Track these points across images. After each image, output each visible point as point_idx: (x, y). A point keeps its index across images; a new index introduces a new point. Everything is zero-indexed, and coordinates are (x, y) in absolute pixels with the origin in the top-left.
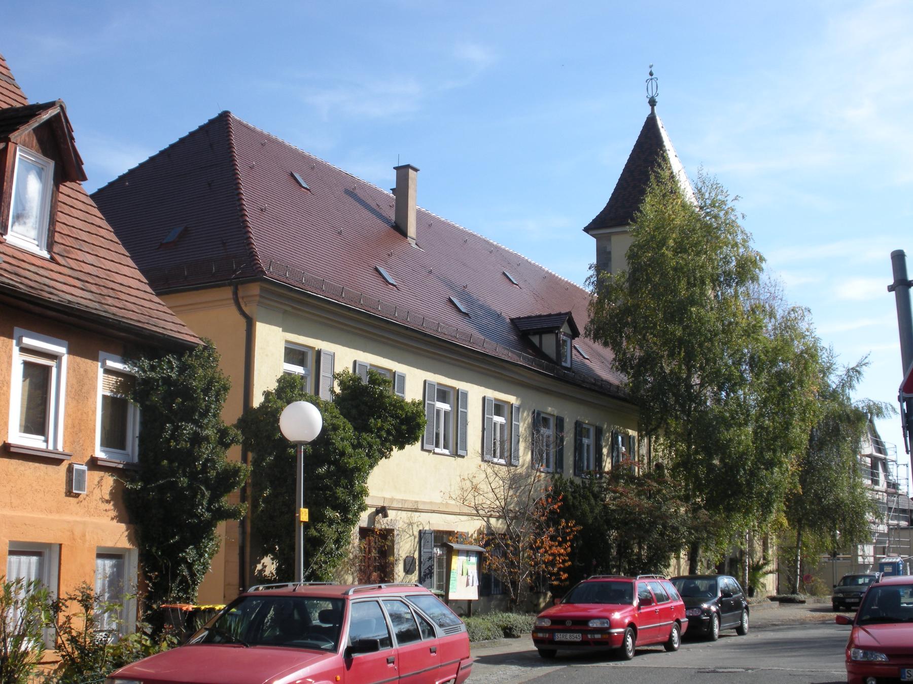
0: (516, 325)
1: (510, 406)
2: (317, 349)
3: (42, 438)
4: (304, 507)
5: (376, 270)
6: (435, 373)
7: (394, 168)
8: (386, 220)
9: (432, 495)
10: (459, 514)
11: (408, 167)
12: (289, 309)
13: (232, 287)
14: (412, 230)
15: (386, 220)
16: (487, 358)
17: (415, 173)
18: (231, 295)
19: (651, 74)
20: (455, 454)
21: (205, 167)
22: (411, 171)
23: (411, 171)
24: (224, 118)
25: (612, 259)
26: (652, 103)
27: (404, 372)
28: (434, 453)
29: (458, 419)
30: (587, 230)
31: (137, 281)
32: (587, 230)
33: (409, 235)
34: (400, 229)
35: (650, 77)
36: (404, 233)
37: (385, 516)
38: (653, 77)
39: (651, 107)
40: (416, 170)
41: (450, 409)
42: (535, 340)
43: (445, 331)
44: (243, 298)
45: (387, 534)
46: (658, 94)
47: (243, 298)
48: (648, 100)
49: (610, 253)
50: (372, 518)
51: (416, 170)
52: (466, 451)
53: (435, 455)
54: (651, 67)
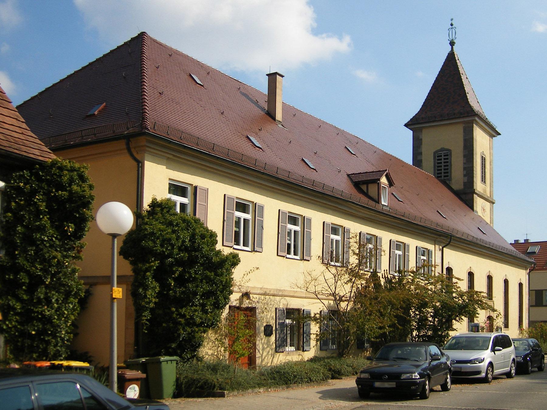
0: (351, 178)
1: (254, 205)
2: (194, 185)
3: (534, 304)
4: (117, 287)
5: (248, 137)
6: (174, 171)
7: (267, 75)
8: (263, 109)
9: (285, 285)
10: (305, 298)
11: (276, 74)
12: (171, 156)
13: (126, 140)
14: (279, 116)
15: (263, 109)
16: (325, 196)
17: (281, 78)
18: (125, 147)
19: (452, 25)
20: (303, 259)
21: (127, 66)
22: (278, 76)
23: (278, 76)
24: (142, 36)
25: (423, 143)
26: (452, 44)
27: (263, 204)
28: (286, 258)
29: (306, 235)
30: (406, 125)
31: (15, 120)
32: (406, 125)
33: (276, 119)
34: (271, 115)
35: (451, 27)
36: (274, 118)
37: (249, 298)
38: (453, 27)
39: (451, 47)
40: (282, 76)
41: (188, 202)
42: (364, 187)
43: (293, 177)
44: (135, 148)
45: (252, 310)
46: (456, 38)
47: (135, 148)
48: (449, 42)
49: (421, 139)
50: (241, 300)
51: (282, 76)
52: (381, 269)
53: (287, 259)
54: (452, 20)
